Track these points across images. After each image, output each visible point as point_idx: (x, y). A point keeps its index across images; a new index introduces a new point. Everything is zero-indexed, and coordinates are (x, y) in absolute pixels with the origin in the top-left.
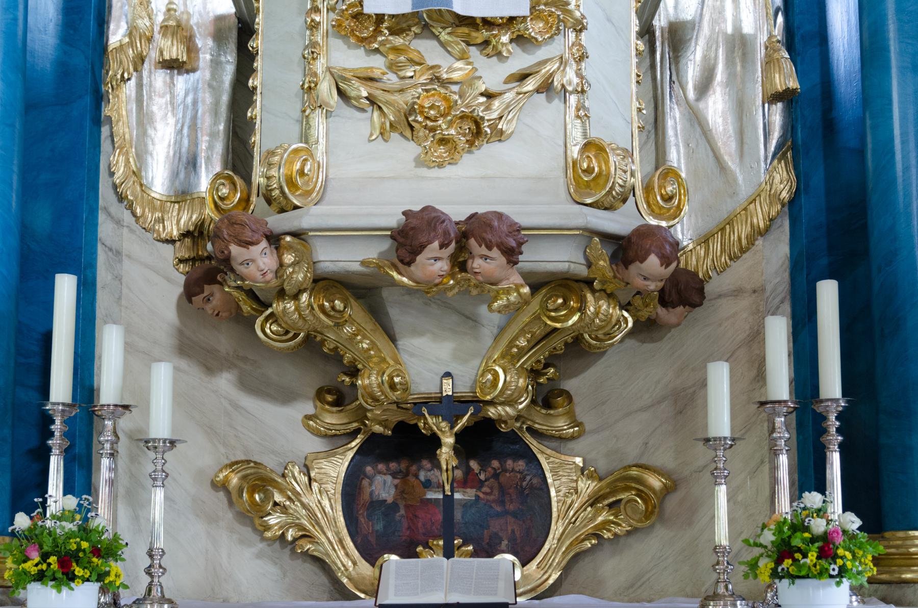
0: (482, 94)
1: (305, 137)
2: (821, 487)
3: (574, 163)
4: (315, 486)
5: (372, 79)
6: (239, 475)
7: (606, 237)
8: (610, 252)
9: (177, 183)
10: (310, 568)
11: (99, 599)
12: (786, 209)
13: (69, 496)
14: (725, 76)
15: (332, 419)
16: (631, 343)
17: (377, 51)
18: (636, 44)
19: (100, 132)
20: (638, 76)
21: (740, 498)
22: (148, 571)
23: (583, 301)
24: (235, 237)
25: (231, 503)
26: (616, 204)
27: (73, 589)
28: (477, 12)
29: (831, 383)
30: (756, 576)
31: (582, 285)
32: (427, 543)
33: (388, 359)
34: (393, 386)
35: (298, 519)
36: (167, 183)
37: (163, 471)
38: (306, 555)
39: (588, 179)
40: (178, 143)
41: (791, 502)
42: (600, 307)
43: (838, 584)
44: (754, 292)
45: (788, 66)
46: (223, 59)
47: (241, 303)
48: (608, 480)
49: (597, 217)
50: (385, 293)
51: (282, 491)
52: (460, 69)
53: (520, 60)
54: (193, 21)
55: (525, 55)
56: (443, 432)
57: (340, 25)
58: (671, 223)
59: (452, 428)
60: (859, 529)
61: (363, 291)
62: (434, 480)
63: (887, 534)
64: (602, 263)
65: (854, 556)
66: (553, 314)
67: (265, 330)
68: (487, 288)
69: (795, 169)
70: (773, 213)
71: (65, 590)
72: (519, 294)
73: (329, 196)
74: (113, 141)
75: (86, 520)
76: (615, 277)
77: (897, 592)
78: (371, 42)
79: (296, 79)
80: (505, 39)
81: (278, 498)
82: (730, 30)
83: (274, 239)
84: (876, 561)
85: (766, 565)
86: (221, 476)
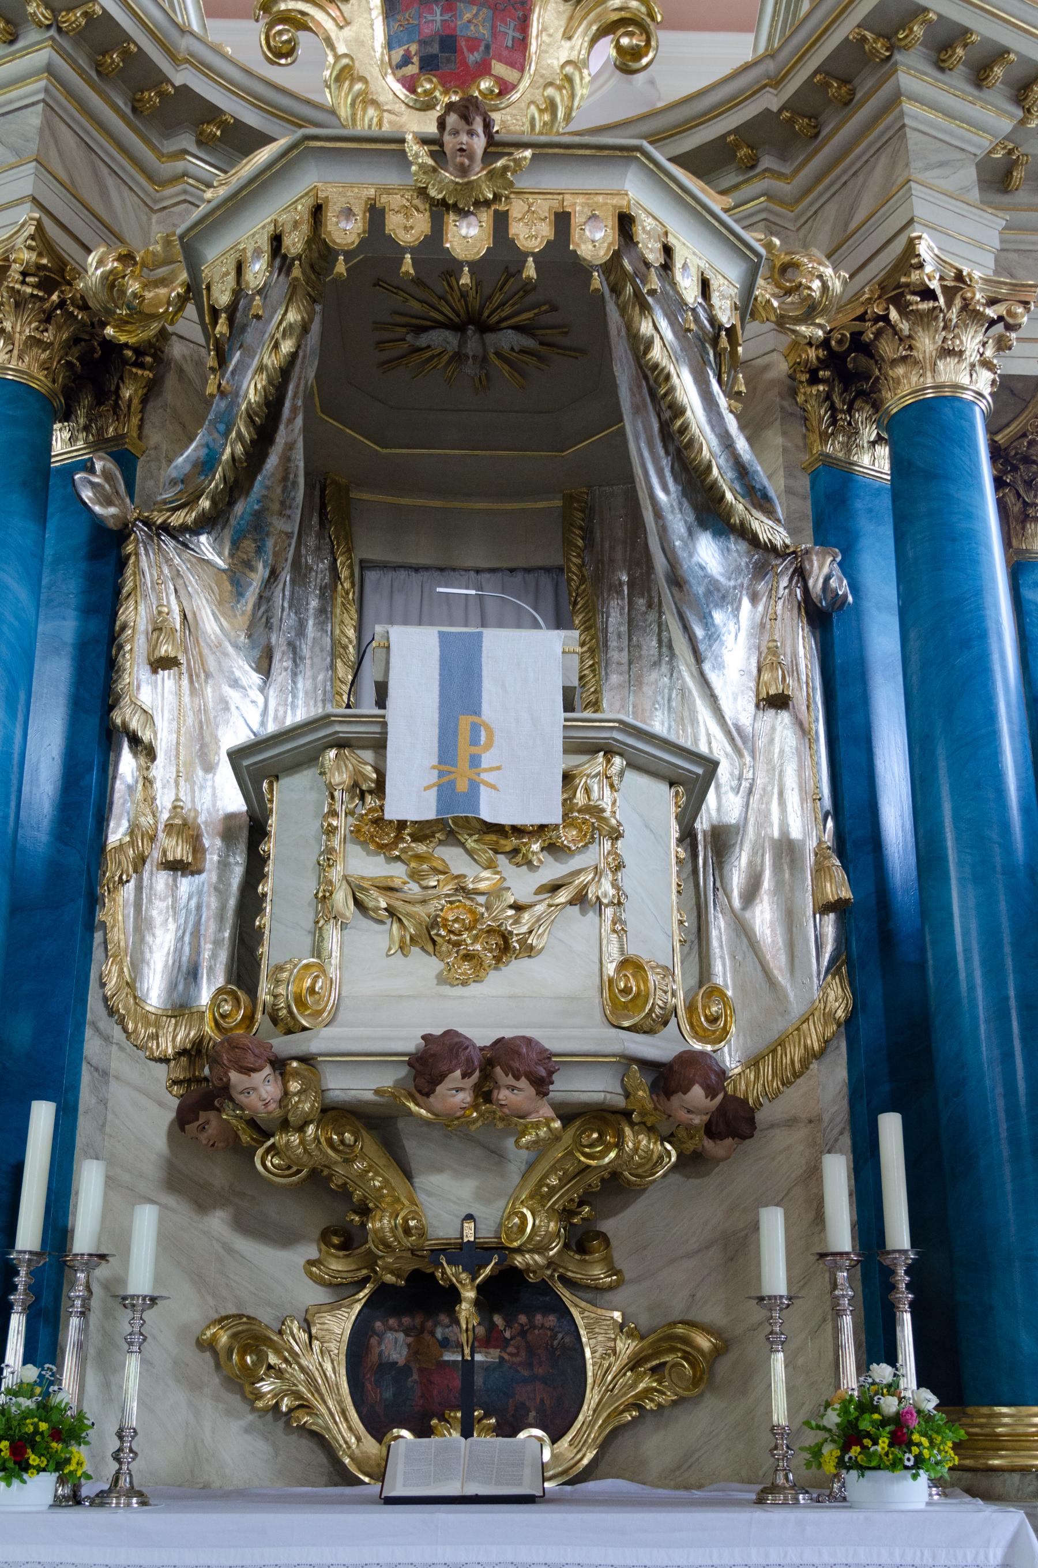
0: (511, 907)
1: (317, 951)
2: (891, 1358)
3: (611, 981)
4: (316, 1344)
5: (391, 889)
6: (229, 1332)
7: (645, 1064)
8: (650, 1080)
9: (175, 995)
10: (306, 1443)
11: (56, 1490)
12: (842, 1029)
13: (30, 1366)
14: (773, 884)
15: (338, 1265)
16: (676, 1178)
17: (398, 858)
18: (675, 850)
19: (92, 938)
20: (679, 885)
21: (800, 1361)
22: (117, 1457)
23: (620, 1135)
24: (236, 1063)
25: (218, 1366)
26: (657, 1027)
27: (25, 1482)
28: (505, 819)
29: (899, 1233)
30: (820, 1466)
31: (619, 1116)
32: (443, 1415)
33: (403, 1199)
34: (407, 1231)
35: (295, 1385)
36: (163, 995)
37: (141, 1334)
38: (303, 1429)
39: (626, 999)
40: (178, 951)
41: (858, 1375)
42: (639, 1142)
43: (915, 1477)
44: (810, 1121)
45: (840, 874)
46: (231, 860)
47: (240, 1133)
48: (651, 1339)
49: (635, 1042)
50: (401, 1124)
51: (278, 1352)
52: (487, 879)
53: (551, 870)
54: (201, 820)
55: (558, 864)
56: (463, 1285)
57: (358, 831)
58: (717, 1047)
59: (473, 1280)
60: (936, 1408)
61: (376, 1123)
62: (453, 1338)
63: (970, 1410)
64: (641, 1093)
65: (931, 1442)
66: (587, 1150)
67: (265, 1163)
68: (515, 1122)
69: (851, 985)
70: (828, 1034)
71: (16, 1483)
72: (550, 1129)
73: (342, 1015)
74: (106, 948)
75: (46, 1394)
76: (656, 1109)
77: (983, 1482)
78: (392, 849)
79: (310, 886)
80: (536, 847)
81: (273, 1359)
82: (776, 834)
83: (279, 1065)
84: (957, 1447)
85: (830, 1452)
86: (209, 1333)
